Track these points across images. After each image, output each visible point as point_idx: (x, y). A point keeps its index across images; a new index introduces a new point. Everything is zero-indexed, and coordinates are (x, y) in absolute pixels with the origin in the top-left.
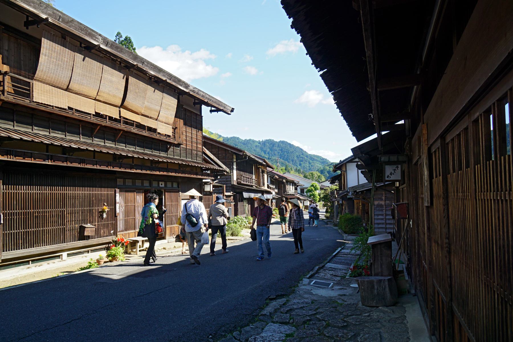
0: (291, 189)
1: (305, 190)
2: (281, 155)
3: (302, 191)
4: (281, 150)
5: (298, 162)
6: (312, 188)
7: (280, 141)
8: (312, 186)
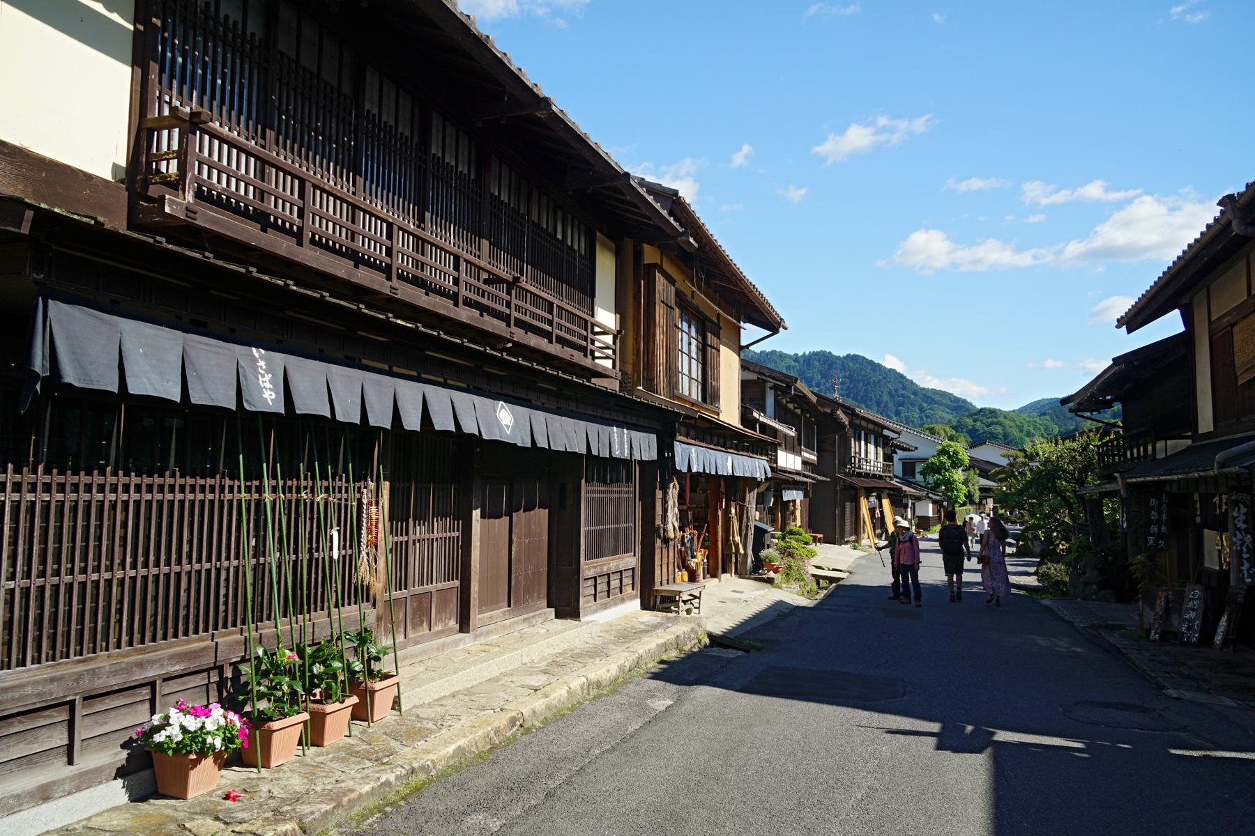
0: (872, 456)
1: (919, 468)
2: (848, 389)
3: (909, 467)
4: (850, 377)
5: (891, 405)
6: (944, 459)
7: (848, 356)
8: (944, 452)
